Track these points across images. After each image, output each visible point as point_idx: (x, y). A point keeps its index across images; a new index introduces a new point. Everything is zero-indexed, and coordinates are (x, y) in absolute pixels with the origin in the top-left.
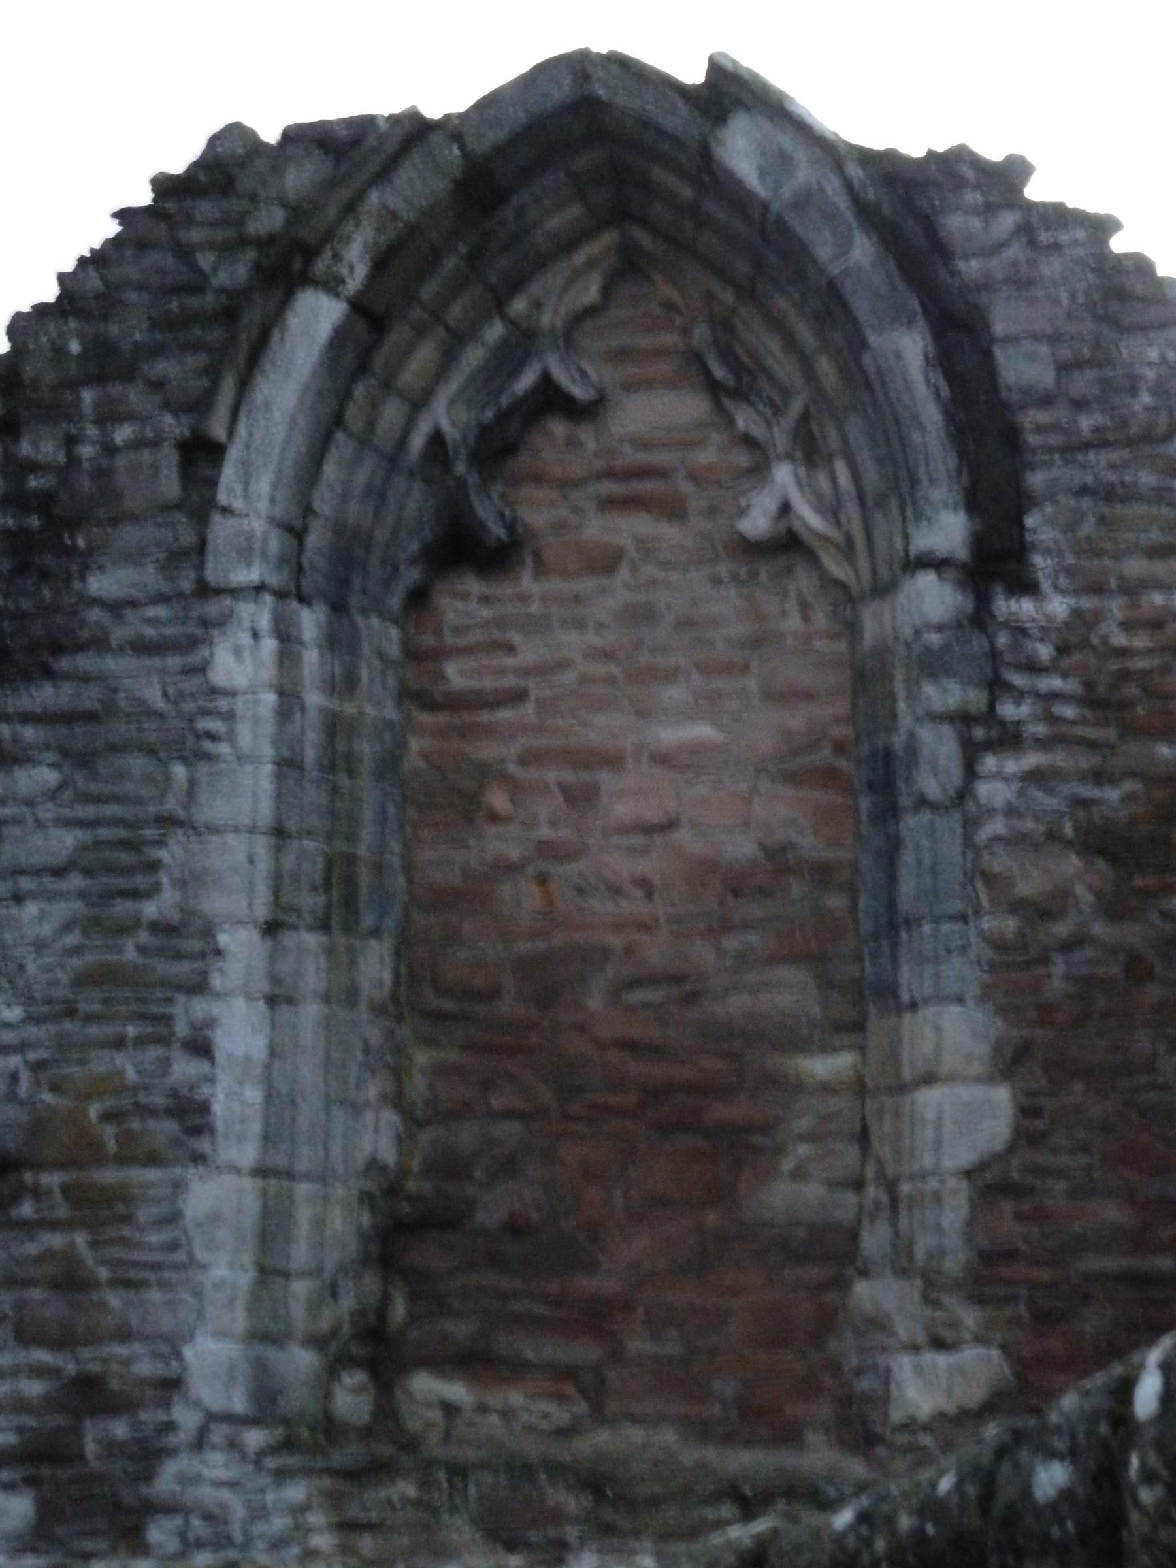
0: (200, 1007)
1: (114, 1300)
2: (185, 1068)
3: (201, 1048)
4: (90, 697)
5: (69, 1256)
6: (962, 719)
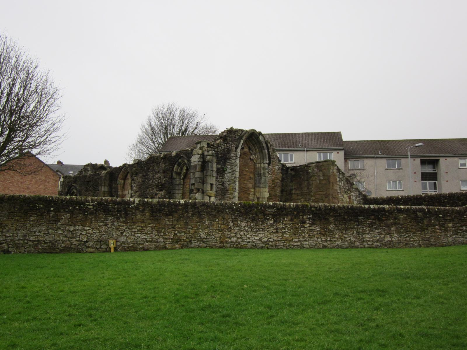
2: (235, 186)
3: (236, 185)
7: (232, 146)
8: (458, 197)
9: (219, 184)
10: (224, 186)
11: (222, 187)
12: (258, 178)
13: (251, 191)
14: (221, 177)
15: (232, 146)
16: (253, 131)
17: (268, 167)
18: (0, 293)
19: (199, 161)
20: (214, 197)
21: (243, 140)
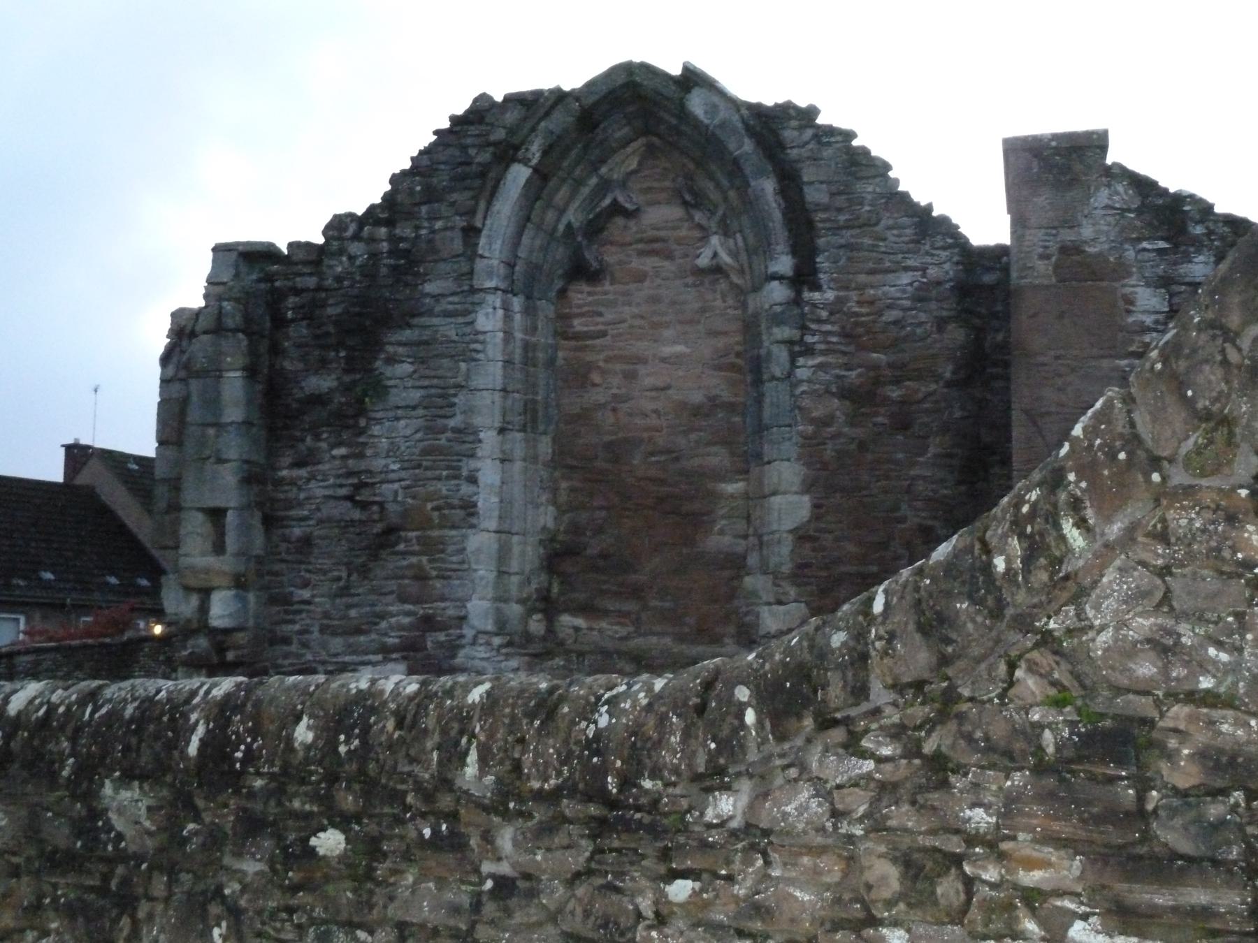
0: (473, 464)
1: (438, 584)
2: (466, 489)
3: (473, 480)
4: (425, 336)
5: (419, 567)
6: (790, 343)
7: (439, 225)
8: (78, 667)
9: (326, 497)
10: (364, 506)
11: (357, 515)
12: (478, 421)
13: (714, 496)
14: (342, 451)
15: (433, 232)
16: (621, 80)
17: (797, 301)
18: (1, 939)
19: (738, 355)
20: (227, 594)
21: (525, 162)
